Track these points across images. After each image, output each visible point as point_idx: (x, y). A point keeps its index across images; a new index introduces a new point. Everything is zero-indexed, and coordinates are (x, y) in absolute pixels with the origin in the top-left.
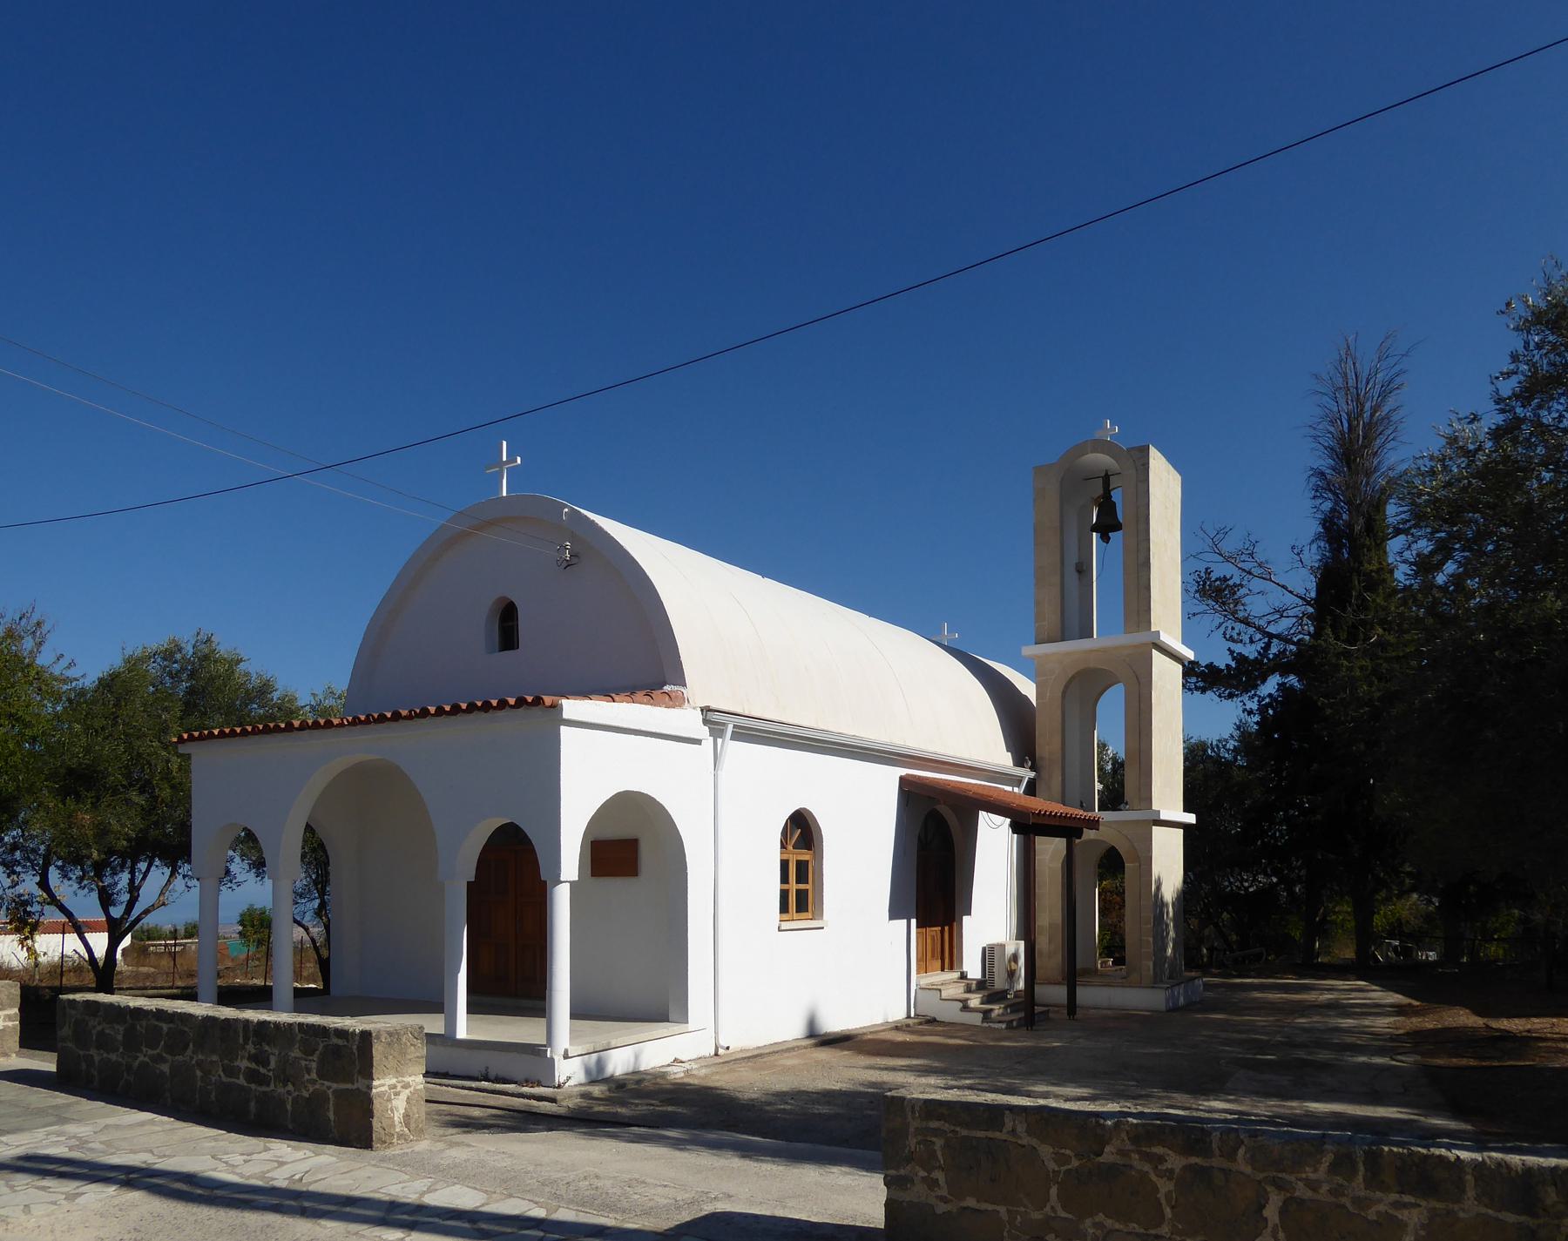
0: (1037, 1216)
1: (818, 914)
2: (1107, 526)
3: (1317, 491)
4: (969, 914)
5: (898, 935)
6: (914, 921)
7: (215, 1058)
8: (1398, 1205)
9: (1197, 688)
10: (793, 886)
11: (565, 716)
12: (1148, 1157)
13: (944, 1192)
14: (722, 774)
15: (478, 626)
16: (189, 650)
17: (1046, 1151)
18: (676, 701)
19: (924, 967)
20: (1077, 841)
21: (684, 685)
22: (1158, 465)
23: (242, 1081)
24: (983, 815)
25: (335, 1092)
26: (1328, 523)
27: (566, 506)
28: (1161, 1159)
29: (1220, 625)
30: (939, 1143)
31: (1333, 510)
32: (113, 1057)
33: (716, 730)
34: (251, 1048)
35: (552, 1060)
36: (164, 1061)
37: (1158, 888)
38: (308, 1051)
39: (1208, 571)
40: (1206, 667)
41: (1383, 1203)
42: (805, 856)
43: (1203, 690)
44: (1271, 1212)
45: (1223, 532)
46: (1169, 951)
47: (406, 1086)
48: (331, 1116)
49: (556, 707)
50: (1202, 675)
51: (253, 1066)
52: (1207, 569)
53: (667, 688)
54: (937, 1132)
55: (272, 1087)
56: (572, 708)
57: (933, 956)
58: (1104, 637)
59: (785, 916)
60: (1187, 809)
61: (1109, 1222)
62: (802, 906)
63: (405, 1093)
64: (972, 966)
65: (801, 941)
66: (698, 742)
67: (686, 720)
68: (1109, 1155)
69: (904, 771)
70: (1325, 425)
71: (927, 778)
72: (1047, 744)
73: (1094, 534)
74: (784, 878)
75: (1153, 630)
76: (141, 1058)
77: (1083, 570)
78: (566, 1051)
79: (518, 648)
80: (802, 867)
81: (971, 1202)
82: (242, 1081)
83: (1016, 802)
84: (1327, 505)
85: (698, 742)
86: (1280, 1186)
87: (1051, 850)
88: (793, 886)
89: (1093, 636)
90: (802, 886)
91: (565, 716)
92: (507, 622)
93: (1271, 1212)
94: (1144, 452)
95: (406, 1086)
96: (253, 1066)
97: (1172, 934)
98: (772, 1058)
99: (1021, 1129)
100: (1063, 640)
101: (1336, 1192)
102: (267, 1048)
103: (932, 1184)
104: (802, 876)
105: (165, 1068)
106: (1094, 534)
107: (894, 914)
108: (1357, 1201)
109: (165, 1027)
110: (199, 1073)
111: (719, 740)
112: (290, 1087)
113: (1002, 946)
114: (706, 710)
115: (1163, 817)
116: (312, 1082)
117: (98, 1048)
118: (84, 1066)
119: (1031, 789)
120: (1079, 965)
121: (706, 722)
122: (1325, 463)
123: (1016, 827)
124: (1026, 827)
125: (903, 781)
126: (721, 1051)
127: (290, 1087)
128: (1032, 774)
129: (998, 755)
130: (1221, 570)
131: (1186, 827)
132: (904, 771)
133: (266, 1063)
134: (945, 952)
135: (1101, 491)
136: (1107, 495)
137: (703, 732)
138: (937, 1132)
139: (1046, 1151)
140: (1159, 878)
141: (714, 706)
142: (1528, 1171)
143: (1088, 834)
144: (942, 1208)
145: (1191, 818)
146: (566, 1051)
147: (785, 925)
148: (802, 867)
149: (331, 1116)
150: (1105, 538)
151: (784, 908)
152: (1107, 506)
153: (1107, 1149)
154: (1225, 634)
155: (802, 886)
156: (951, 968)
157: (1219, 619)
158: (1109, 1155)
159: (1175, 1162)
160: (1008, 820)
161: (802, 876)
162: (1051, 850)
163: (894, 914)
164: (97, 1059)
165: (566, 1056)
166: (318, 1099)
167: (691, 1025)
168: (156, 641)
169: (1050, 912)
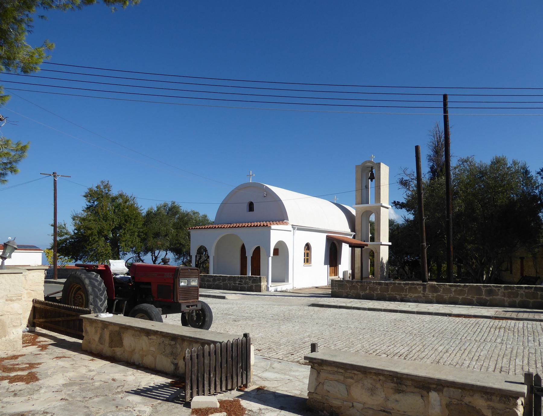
0: (347, 291)
1: (311, 263)
2: (372, 178)
3: (429, 160)
4: (340, 264)
5: (325, 269)
6: (329, 265)
7: (232, 282)
8: (378, 286)
9: (399, 208)
10: (306, 258)
11: (272, 228)
12: (357, 284)
13: (337, 289)
14: (294, 237)
15: (246, 207)
16: (170, 206)
17: (348, 284)
18: (287, 224)
19: (331, 275)
20: (363, 249)
21: (288, 220)
22: (383, 166)
23: (237, 285)
24: (343, 244)
25: (255, 285)
26: (432, 168)
27: (265, 185)
28: (358, 284)
29: (406, 192)
30: (337, 284)
31: (433, 165)
32: (210, 283)
33: (294, 229)
34: (239, 280)
35: (269, 287)
36: (222, 283)
37: (382, 260)
38: (250, 280)
39: (402, 179)
40: (402, 203)
41: (377, 286)
42: (308, 252)
43: (401, 208)
44: (368, 288)
45: (406, 169)
46: (385, 274)
47: (264, 284)
48: (254, 288)
49: (270, 227)
50: (400, 205)
51: (240, 282)
52: (402, 178)
53: (285, 221)
54: (337, 283)
55: (243, 285)
56: (273, 227)
57: (332, 273)
58: (372, 202)
59: (305, 263)
60: (389, 242)
61: (354, 291)
62: (307, 262)
63: (264, 285)
64: (341, 275)
65: (307, 269)
66: (291, 231)
67: (289, 227)
68: (354, 284)
69: (327, 234)
70: (431, 144)
71: (332, 236)
72: (358, 227)
73: (370, 180)
74: (305, 256)
75: (381, 203)
76: (216, 283)
77: (367, 187)
78: (271, 286)
79: (253, 211)
80: (308, 254)
81: (340, 290)
82: (237, 285)
83: (350, 241)
84: (431, 164)
85: (291, 231)
86: (369, 286)
87: (358, 251)
88: (306, 258)
89: (369, 204)
90: (308, 258)
91: (272, 228)
92: (251, 206)
93: (368, 288)
94: (380, 163)
95: (264, 284)
96: (240, 282)
97: (386, 270)
98: (303, 290)
99: (345, 282)
100: (362, 204)
101: (373, 286)
102: (242, 280)
103: (336, 289)
104: (307, 256)
105: (222, 284)
106: (370, 180)
107: (325, 264)
108: (375, 286)
109: (221, 278)
110: (229, 284)
111: (294, 230)
112: (246, 285)
113: (347, 271)
114: (292, 225)
115: (382, 244)
116: (251, 284)
117: (207, 282)
118: (204, 285)
119: (354, 237)
120: (364, 276)
121: (292, 227)
122: (432, 153)
123: (350, 246)
124: (353, 246)
125: (327, 236)
126: (294, 288)
127: (246, 285)
128: (355, 234)
129: (347, 230)
130: (406, 178)
131: (389, 246)
132: (327, 234)
133: (242, 282)
134: (336, 273)
135: (371, 170)
136: (372, 172)
137: (292, 229)
138: (337, 283)
139: (348, 284)
140: (382, 258)
141: (294, 225)
142: (387, 283)
143: (365, 247)
144: (337, 291)
145: (390, 244)
146: (271, 286)
147: (305, 265)
148: (308, 254)
149: (254, 288)
150: (372, 181)
151: (304, 262)
152: (372, 174)
153: (354, 284)
154: (406, 195)
155: (308, 258)
156: (336, 276)
157: (405, 190)
158: (354, 284)
159: (360, 284)
160: (348, 245)
161: (307, 256)
162: (358, 251)
163: (325, 264)
164: (207, 284)
165: (271, 287)
166: (252, 286)
167: (289, 283)
168: (160, 203)
169: (358, 264)
